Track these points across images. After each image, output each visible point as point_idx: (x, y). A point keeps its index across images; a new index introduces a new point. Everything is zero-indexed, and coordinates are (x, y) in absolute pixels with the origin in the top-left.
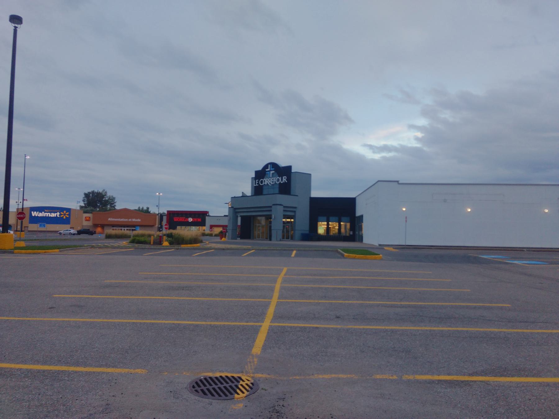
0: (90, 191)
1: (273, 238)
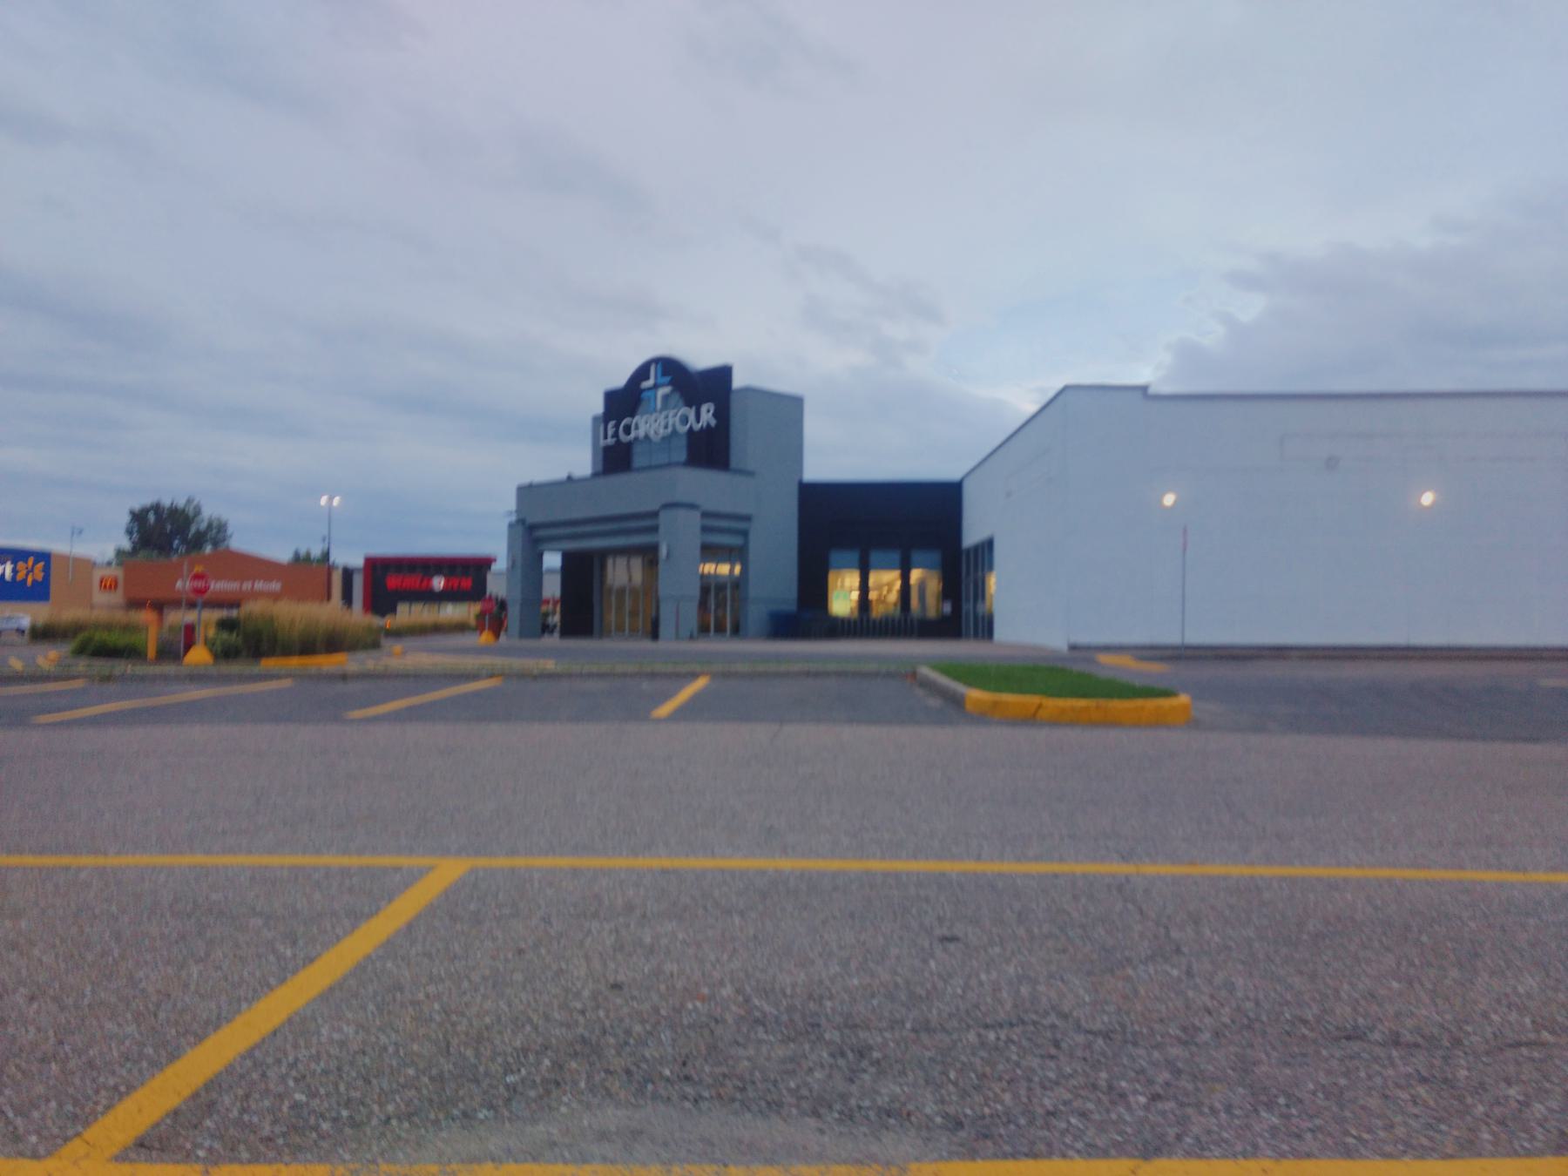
1: (663, 630)
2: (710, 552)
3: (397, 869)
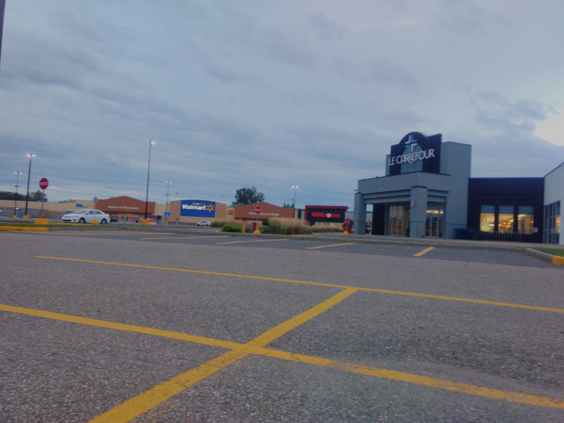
0: (241, 188)
1: (411, 233)
2: (431, 205)
3: (334, 288)
